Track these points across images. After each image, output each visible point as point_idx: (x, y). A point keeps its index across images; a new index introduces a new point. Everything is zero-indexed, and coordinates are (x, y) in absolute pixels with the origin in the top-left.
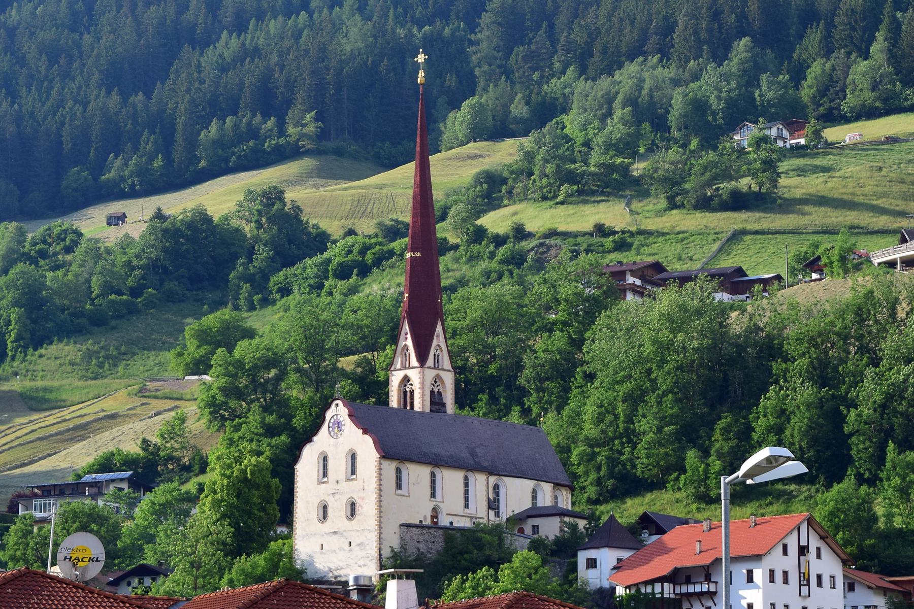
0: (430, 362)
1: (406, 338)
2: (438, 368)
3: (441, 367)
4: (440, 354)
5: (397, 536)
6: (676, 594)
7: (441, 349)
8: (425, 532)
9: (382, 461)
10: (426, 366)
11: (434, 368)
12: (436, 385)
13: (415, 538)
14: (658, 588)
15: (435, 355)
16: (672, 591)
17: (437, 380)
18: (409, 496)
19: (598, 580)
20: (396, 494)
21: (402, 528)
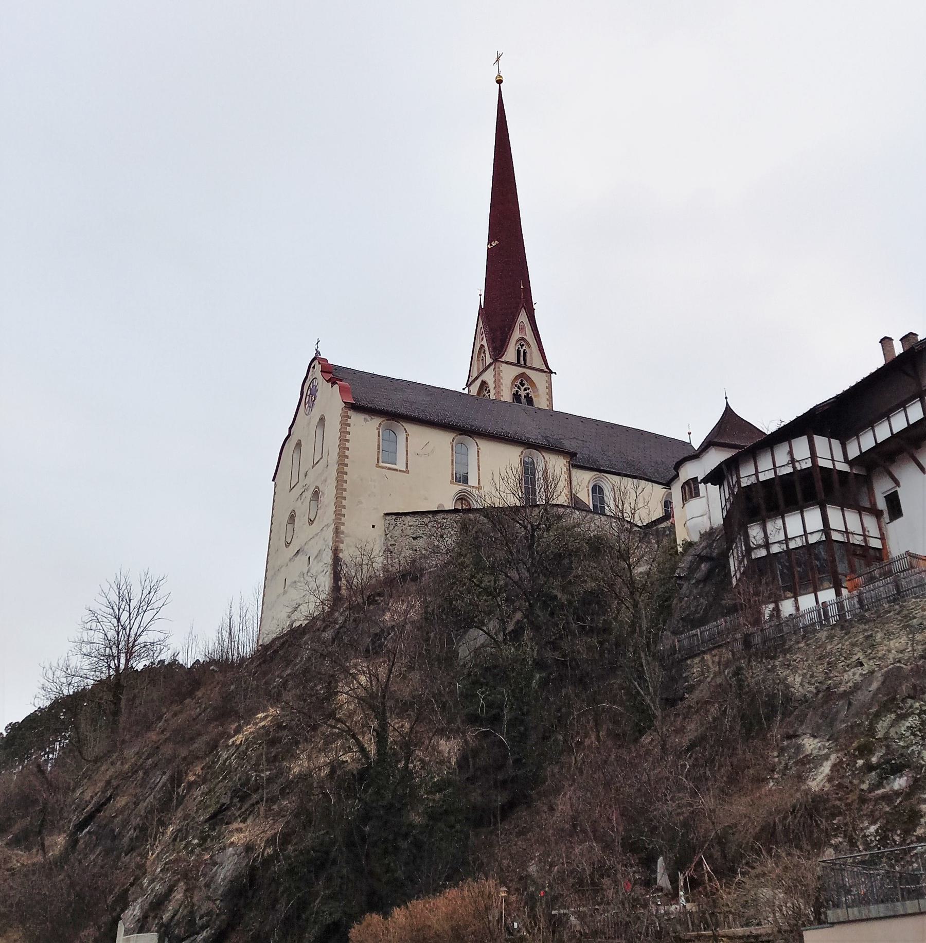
0: (510, 354)
1: (482, 339)
2: (525, 366)
3: (528, 364)
4: (527, 350)
5: (379, 532)
6: (851, 463)
7: (528, 344)
8: (426, 520)
9: (350, 413)
10: (503, 359)
11: (518, 364)
12: (523, 388)
13: (409, 532)
14: (801, 448)
15: (519, 352)
16: (838, 456)
17: (524, 382)
18: (407, 472)
19: (705, 518)
20: (378, 466)
21: (388, 518)
